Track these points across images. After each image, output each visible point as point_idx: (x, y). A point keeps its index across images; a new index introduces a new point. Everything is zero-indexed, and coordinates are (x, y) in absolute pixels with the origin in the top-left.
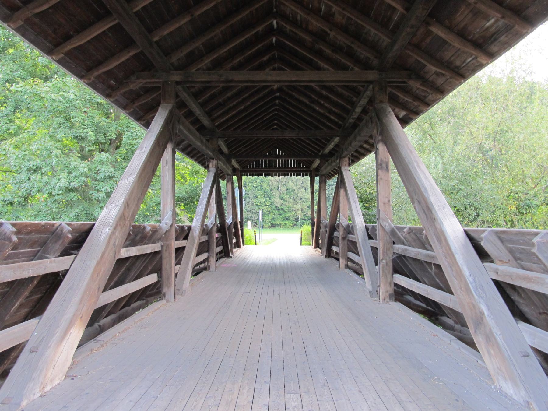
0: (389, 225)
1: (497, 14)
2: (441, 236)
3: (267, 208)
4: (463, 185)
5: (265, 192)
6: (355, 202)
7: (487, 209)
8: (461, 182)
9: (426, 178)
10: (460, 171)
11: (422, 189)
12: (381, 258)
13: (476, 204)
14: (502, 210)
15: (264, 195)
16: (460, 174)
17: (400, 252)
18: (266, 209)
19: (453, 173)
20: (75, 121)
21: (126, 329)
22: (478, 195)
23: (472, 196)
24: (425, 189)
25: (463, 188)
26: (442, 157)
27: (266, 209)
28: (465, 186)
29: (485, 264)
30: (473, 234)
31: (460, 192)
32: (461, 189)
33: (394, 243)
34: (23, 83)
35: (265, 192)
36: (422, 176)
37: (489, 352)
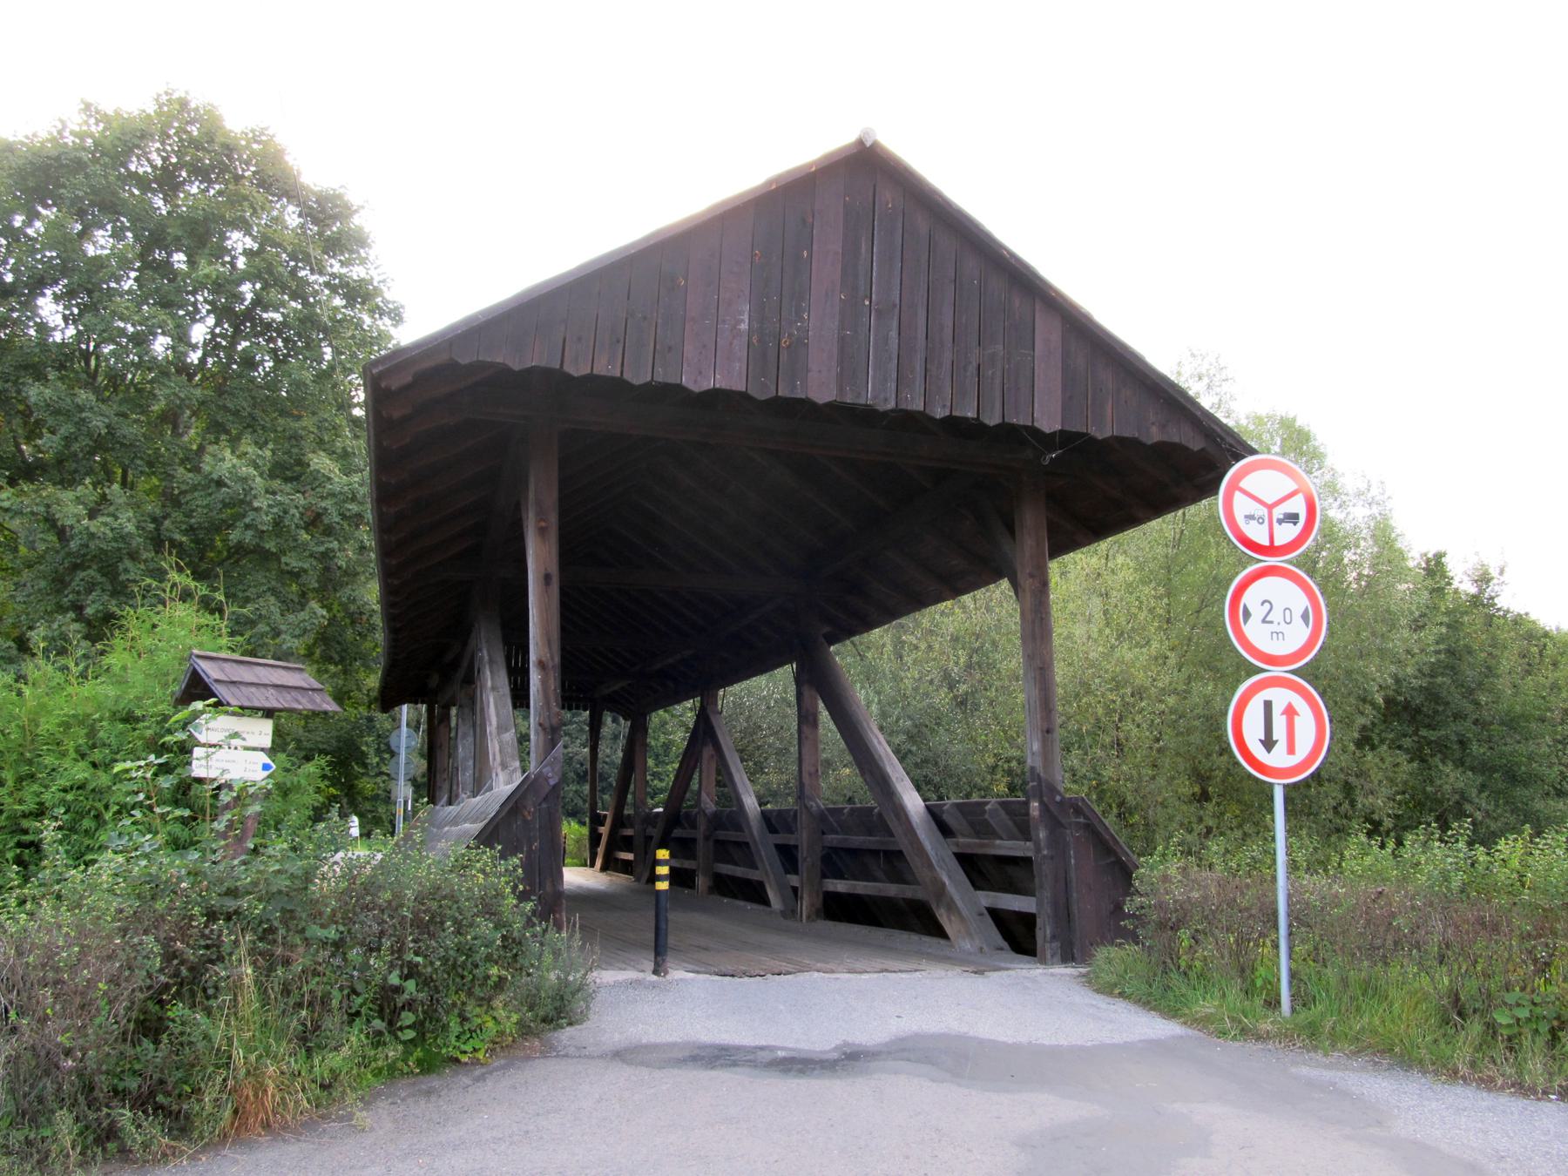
0: (818, 806)
1: (934, 862)
2: (900, 811)
3: (384, 782)
4: (915, 743)
5: (379, 736)
6: (738, 771)
7: (957, 789)
8: (911, 738)
9: (880, 743)
10: (910, 718)
11: (876, 757)
12: (805, 855)
13: (937, 779)
14: (983, 793)
15: (379, 744)
16: (909, 723)
17: (835, 844)
18: (382, 785)
19: (897, 721)
20: (128, 580)
21: (1048, 732)
22: (942, 763)
23: (930, 765)
24: (880, 756)
25: (914, 748)
26: (878, 693)
27: (382, 785)
28: (918, 746)
29: (948, 840)
30: (935, 810)
31: (909, 756)
32: (910, 751)
33: (823, 833)
34: (12, 490)
35: (379, 736)
36: (875, 741)
37: (950, 920)
